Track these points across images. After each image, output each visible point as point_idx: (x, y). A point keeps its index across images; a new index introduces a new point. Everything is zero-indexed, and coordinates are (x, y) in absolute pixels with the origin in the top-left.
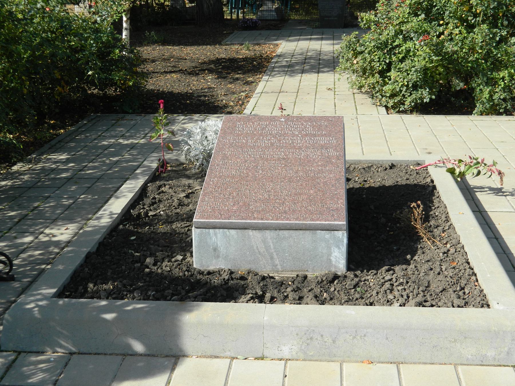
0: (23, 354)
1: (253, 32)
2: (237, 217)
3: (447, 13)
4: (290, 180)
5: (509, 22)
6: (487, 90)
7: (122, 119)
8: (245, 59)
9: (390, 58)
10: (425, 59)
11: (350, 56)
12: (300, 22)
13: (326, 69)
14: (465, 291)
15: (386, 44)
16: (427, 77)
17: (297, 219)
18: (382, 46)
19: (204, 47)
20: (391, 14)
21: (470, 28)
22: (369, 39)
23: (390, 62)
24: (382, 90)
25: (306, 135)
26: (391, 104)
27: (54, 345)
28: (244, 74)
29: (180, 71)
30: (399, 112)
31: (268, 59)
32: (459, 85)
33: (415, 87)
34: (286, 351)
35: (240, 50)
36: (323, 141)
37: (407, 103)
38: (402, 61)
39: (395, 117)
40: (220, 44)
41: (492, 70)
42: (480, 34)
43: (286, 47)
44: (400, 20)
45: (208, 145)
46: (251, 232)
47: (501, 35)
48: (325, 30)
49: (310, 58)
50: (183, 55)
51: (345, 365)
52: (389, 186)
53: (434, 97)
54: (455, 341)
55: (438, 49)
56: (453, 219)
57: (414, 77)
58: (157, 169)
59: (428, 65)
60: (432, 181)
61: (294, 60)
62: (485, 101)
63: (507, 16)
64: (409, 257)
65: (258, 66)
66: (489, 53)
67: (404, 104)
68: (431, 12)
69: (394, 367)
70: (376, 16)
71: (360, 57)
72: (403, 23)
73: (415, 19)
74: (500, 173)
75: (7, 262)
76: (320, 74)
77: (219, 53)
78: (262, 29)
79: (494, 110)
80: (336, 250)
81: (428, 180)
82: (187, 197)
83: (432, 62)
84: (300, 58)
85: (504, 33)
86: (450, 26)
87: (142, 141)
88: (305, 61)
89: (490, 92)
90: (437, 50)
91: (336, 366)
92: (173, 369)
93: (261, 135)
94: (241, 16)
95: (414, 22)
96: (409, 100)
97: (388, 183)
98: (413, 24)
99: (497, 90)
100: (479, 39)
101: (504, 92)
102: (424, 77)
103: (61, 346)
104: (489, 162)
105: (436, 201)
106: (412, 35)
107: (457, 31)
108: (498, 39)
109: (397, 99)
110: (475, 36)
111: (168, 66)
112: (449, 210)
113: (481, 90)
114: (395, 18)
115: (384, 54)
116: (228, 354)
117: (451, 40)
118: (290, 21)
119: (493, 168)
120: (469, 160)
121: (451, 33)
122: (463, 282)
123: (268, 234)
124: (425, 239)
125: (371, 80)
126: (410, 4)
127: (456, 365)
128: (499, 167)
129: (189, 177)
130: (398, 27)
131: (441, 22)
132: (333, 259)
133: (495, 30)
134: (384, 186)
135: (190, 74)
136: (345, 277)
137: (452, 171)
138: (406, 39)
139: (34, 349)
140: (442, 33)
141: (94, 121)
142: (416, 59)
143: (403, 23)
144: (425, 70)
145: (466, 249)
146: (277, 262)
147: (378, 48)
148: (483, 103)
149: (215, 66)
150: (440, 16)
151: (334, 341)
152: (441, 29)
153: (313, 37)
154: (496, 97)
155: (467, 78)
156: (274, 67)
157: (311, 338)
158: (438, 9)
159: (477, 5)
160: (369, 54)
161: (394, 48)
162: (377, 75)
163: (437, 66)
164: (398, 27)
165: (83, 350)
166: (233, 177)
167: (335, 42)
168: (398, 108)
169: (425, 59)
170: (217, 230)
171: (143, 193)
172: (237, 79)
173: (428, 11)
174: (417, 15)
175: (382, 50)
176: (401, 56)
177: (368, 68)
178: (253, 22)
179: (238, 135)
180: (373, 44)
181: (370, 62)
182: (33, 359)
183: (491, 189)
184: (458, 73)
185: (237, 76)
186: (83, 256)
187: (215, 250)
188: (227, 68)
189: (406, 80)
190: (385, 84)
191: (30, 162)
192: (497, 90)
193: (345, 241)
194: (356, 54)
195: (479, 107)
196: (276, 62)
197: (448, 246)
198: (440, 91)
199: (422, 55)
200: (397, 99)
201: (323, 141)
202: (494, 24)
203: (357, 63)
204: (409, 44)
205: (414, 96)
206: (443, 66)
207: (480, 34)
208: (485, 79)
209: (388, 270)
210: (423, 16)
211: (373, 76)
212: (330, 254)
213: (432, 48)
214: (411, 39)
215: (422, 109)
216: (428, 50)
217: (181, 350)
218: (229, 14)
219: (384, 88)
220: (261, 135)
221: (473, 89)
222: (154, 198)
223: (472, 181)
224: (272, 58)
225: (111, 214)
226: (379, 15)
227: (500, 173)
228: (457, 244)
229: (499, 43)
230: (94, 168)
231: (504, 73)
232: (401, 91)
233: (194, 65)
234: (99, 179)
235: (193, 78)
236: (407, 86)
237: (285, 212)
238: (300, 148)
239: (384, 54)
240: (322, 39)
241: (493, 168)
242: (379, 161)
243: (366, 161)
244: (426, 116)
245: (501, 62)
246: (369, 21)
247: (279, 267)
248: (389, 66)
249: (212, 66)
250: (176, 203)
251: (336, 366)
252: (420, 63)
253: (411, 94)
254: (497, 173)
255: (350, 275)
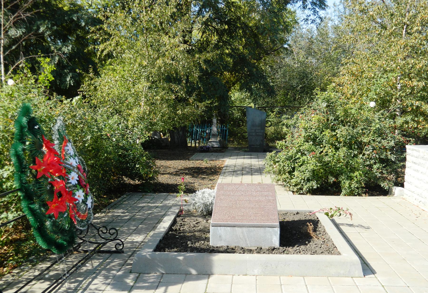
0: (141, 274)
1: (207, 153)
2: (231, 222)
3: (324, 141)
4: (252, 208)
5: (358, 146)
6: (347, 182)
7: (146, 195)
8: (206, 168)
9: (294, 165)
10: (313, 165)
11: (272, 164)
12: (236, 149)
13: (256, 173)
14: (331, 250)
15: (292, 157)
16: (315, 175)
17: (257, 222)
18: (289, 158)
19: (179, 161)
20: (294, 142)
21: (337, 149)
22: (282, 155)
23: (294, 167)
24: (290, 182)
25: (258, 191)
26: (295, 190)
27: (155, 271)
28: (207, 175)
29: (168, 173)
30: (300, 194)
31: (220, 168)
32: (332, 179)
33: (308, 180)
34: (256, 272)
35: (204, 163)
36: (266, 193)
37: (304, 189)
38: (300, 166)
39: (297, 196)
40: (189, 160)
41: (350, 172)
42: (343, 152)
43: (229, 162)
44: (299, 144)
45: (206, 200)
46: (236, 228)
47: (354, 154)
48: (252, 153)
49: (246, 168)
50: (168, 165)
51: (281, 277)
52: (297, 221)
53: (319, 186)
54: (327, 266)
55: (320, 159)
56: (327, 230)
57: (308, 175)
58: (178, 213)
59: (315, 168)
60: (318, 218)
61: (236, 169)
62: (347, 188)
63: (357, 143)
64: (307, 242)
65: (214, 172)
66: (348, 162)
67: (302, 190)
68: (316, 141)
69: (302, 278)
70: (285, 143)
71: (277, 164)
72: (300, 146)
73: (307, 143)
74: (350, 214)
75: (121, 243)
76: (253, 176)
77: (190, 165)
78: (212, 152)
79: (351, 193)
80: (275, 237)
81: (316, 218)
82: (197, 224)
83: (317, 166)
84: (240, 168)
85: (356, 152)
86: (326, 148)
87: (161, 205)
88: (243, 169)
89: (349, 184)
90: (319, 160)
91: (278, 277)
92: (209, 278)
93: (236, 191)
94: (197, 145)
95: (307, 146)
96: (305, 187)
97: (296, 219)
98: (306, 146)
99: (353, 182)
100: (342, 155)
101: (357, 184)
102: (313, 175)
103: (158, 271)
104: (345, 209)
105: (319, 226)
106: (306, 152)
107: (330, 151)
108: (352, 155)
109: (299, 187)
110: (340, 153)
111: (167, 169)
112: (325, 228)
113: (344, 182)
114: (296, 144)
115: (291, 162)
116: (231, 273)
117: (327, 155)
118: (229, 148)
119: (347, 212)
120: (335, 209)
121: (327, 152)
122: (331, 250)
123: (244, 229)
124: (314, 238)
125: (284, 176)
126: (304, 136)
127: (328, 277)
128: (350, 211)
129: (195, 217)
130: (298, 148)
131: (321, 146)
132: (273, 241)
133: (351, 151)
134: (294, 221)
135: (175, 175)
136: (279, 249)
137: (327, 214)
138: (303, 154)
139: (146, 272)
140: (322, 152)
141: (130, 196)
142: (308, 165)
143: (300, 146)
144: (313, 171)
145: (333, 240)
146: (248, 243)
147: (287, 159)
148: (345, 189)
149: (188, 171)
150: (321, 143)
151: (276, 267)
152: (322, 150)
153: (245, 157)
154: (352, 186)
155: (336, 177)
156: (225, 172)
157: (267, 266)
158: (319, 139)
159: (340, 137)
160: (282, 162)
161: (295, 160)
162: (287, 174)
163: (320, 169)
164: (298, 148)
165: (167, 272)
166: (226, 207)
167: (259, 160)
168: (300, 191)
169: (313, 165)
170: (221, 227)
171: (174, 222)
172: (204, 178)
173: (314, 140)
174: (308, 142)
175: (290, 160)
176: (300, 164)
177: (282, 170)
178: (207, 148)
179: (225, 191)
180: (284, 157)
181: (283, 167)
182: (146, 275)
183: (347, 224)
184: (332, 174)
185: (204, 176)
186: (159, 240)
187: (220, 237)
188: (197, 172)
189: (303, 176)
190: (292, 178)
191: (104, 212)
192: (353, 182)
193: (279, 232)
194: (275, 162)
195: (344, 192)
196: (225, 170)
197: (325, 240)
198: (322, 184)
199: (311, 164)
200: (299, 187)
201: (266, 193)
202: (350, 148)
203: (276, 167)
204: (304, 157)
205: (308, 185)
206: (323, 169)
207: (343, 152)
208: (346, 176)
209: (298, 247)
210: (312, 143)
211: (285, 174)
212: (272, 239)
213: (317, 159)
214: (306, 155)
215: (313, 192)
216: (314, 161)
217: (211, 272)
218: (191, 143)
219: (291, 181)
220: (236, 191)
221: (340, 182)
222: (181, 223)
223: (338, 220)
224: (222, 168)
225: (164, 228)
226: (287, 142)
227: (350, 214)
228: (329, 240)
229: (353, 157)
230: (140, 215)
231: (357, 173)
232: (301, 182)
233: (175, 170)
234: (145, 219)
235: (178, 177)
236: (304, 179)
237: (252, 220)
238: (255, 196)
239: (291, 162)
240: (251, 158)
241: (347, 212)
242: (291, 211)
243: (285, 210)
244: (314, 196)
245: (355, 168)
246: (282, 146)
247: (249, 245)
248: (294, 169)
249: (187, 171)
250: (192, 225)
251: (278, 277)
252: (311, 167)
253: (306, 184)
254: (349, 214)
255: (281, 248)
